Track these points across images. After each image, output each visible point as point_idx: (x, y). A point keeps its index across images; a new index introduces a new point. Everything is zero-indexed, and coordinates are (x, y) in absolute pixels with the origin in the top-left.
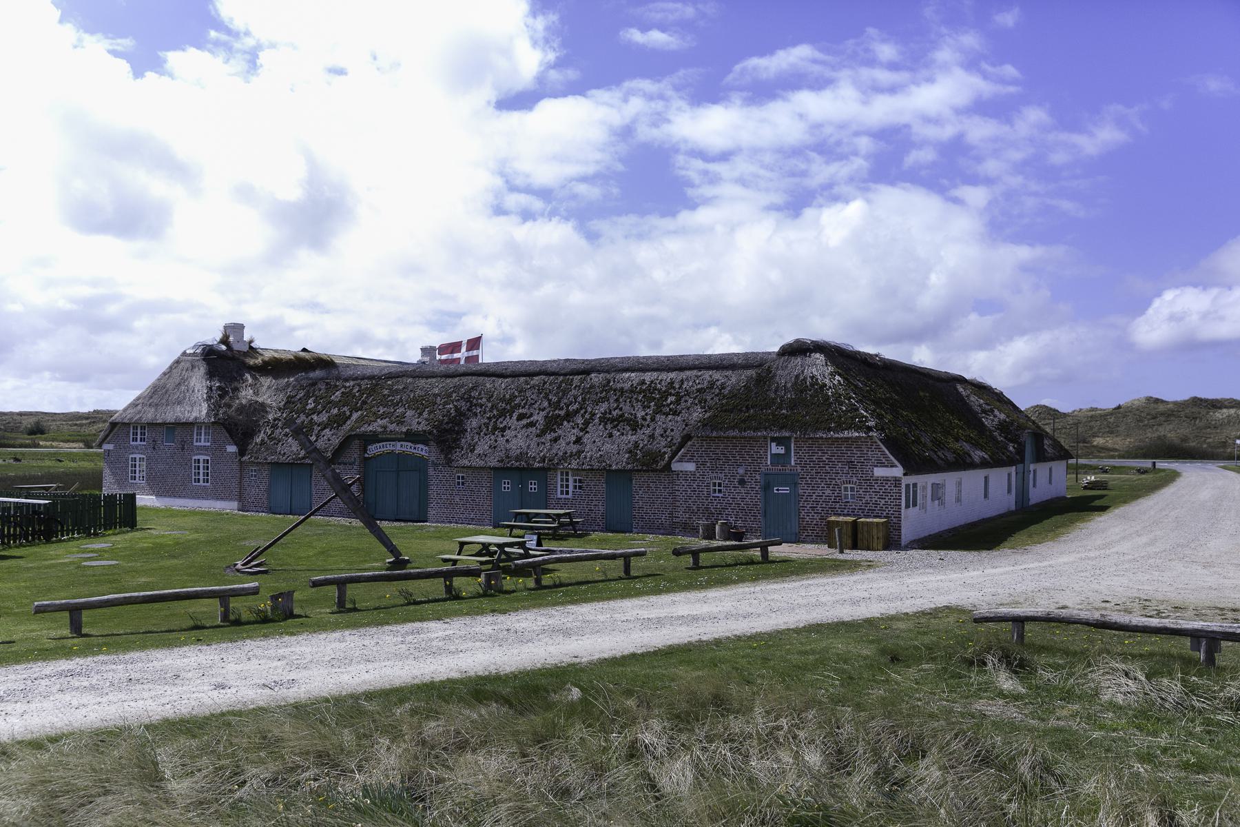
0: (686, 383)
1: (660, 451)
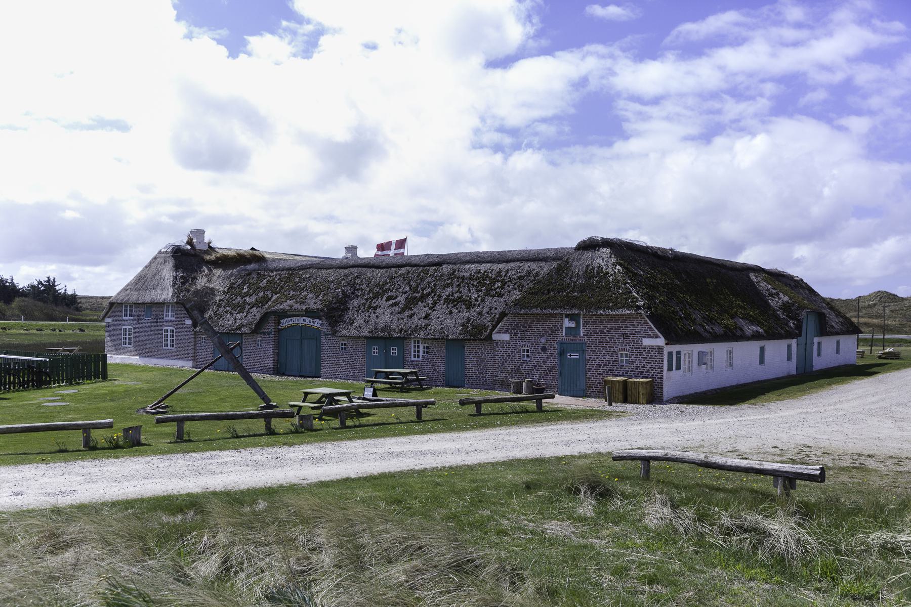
0: (510, 272)
1: (485, 325)
